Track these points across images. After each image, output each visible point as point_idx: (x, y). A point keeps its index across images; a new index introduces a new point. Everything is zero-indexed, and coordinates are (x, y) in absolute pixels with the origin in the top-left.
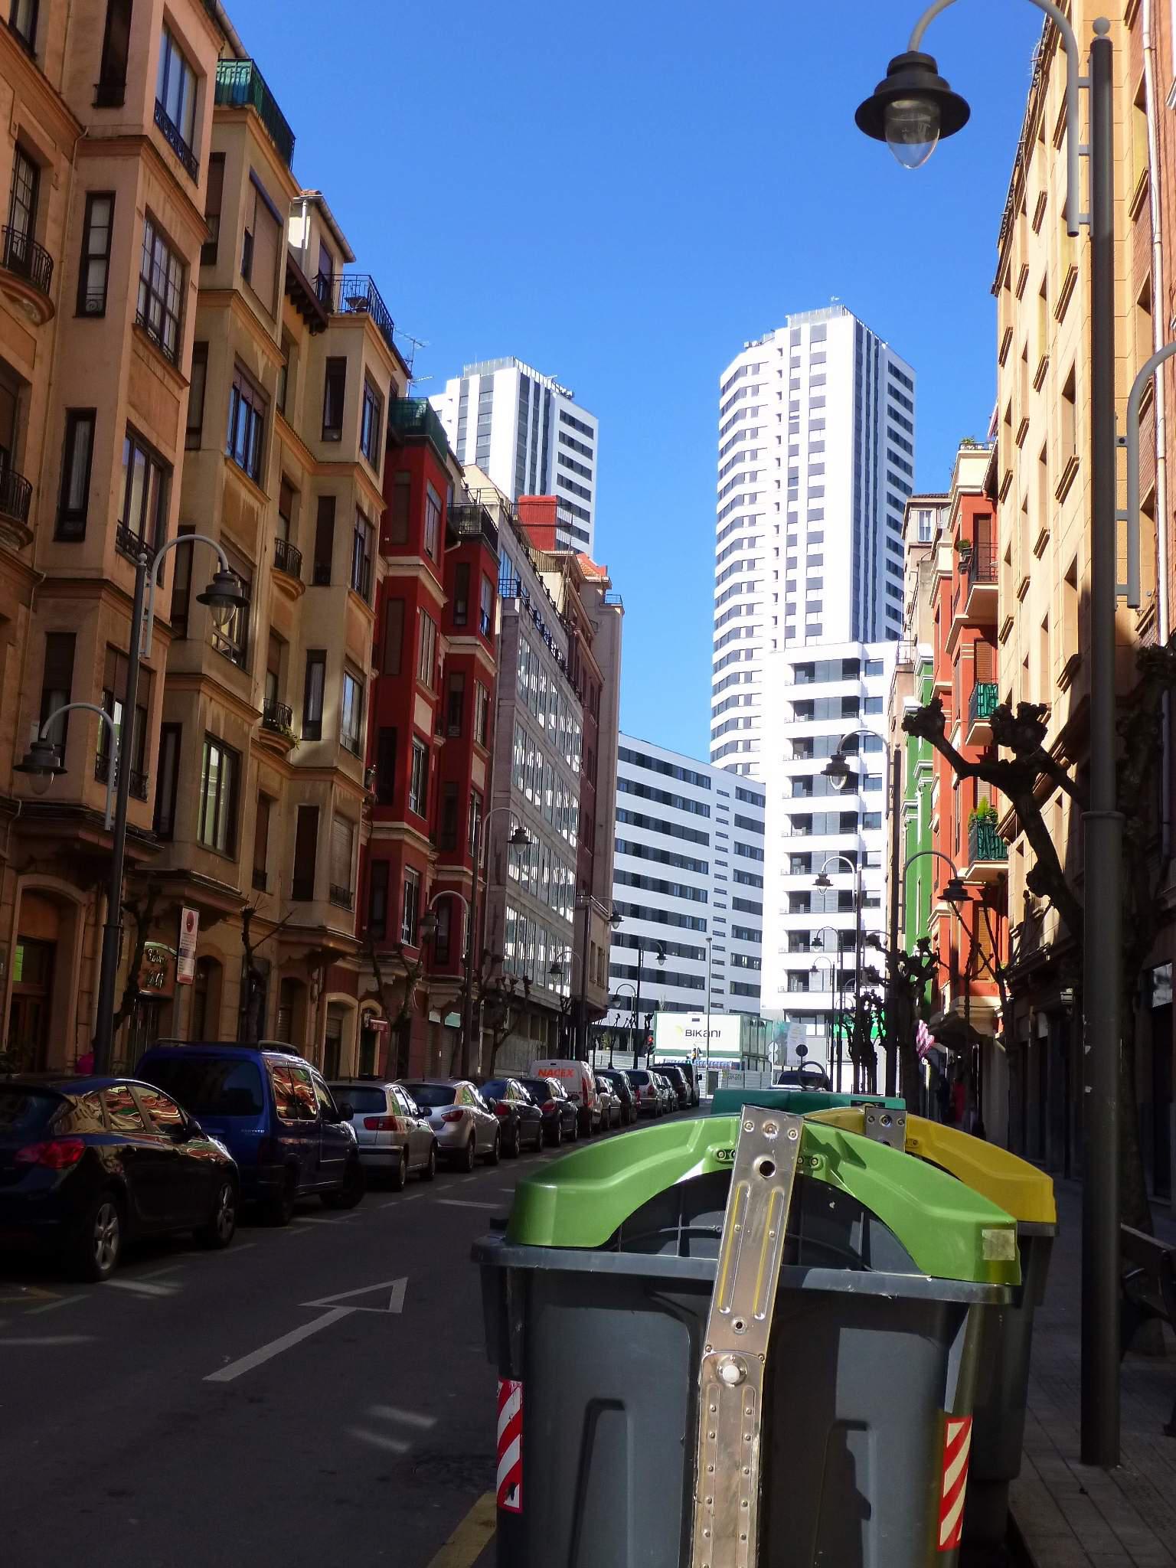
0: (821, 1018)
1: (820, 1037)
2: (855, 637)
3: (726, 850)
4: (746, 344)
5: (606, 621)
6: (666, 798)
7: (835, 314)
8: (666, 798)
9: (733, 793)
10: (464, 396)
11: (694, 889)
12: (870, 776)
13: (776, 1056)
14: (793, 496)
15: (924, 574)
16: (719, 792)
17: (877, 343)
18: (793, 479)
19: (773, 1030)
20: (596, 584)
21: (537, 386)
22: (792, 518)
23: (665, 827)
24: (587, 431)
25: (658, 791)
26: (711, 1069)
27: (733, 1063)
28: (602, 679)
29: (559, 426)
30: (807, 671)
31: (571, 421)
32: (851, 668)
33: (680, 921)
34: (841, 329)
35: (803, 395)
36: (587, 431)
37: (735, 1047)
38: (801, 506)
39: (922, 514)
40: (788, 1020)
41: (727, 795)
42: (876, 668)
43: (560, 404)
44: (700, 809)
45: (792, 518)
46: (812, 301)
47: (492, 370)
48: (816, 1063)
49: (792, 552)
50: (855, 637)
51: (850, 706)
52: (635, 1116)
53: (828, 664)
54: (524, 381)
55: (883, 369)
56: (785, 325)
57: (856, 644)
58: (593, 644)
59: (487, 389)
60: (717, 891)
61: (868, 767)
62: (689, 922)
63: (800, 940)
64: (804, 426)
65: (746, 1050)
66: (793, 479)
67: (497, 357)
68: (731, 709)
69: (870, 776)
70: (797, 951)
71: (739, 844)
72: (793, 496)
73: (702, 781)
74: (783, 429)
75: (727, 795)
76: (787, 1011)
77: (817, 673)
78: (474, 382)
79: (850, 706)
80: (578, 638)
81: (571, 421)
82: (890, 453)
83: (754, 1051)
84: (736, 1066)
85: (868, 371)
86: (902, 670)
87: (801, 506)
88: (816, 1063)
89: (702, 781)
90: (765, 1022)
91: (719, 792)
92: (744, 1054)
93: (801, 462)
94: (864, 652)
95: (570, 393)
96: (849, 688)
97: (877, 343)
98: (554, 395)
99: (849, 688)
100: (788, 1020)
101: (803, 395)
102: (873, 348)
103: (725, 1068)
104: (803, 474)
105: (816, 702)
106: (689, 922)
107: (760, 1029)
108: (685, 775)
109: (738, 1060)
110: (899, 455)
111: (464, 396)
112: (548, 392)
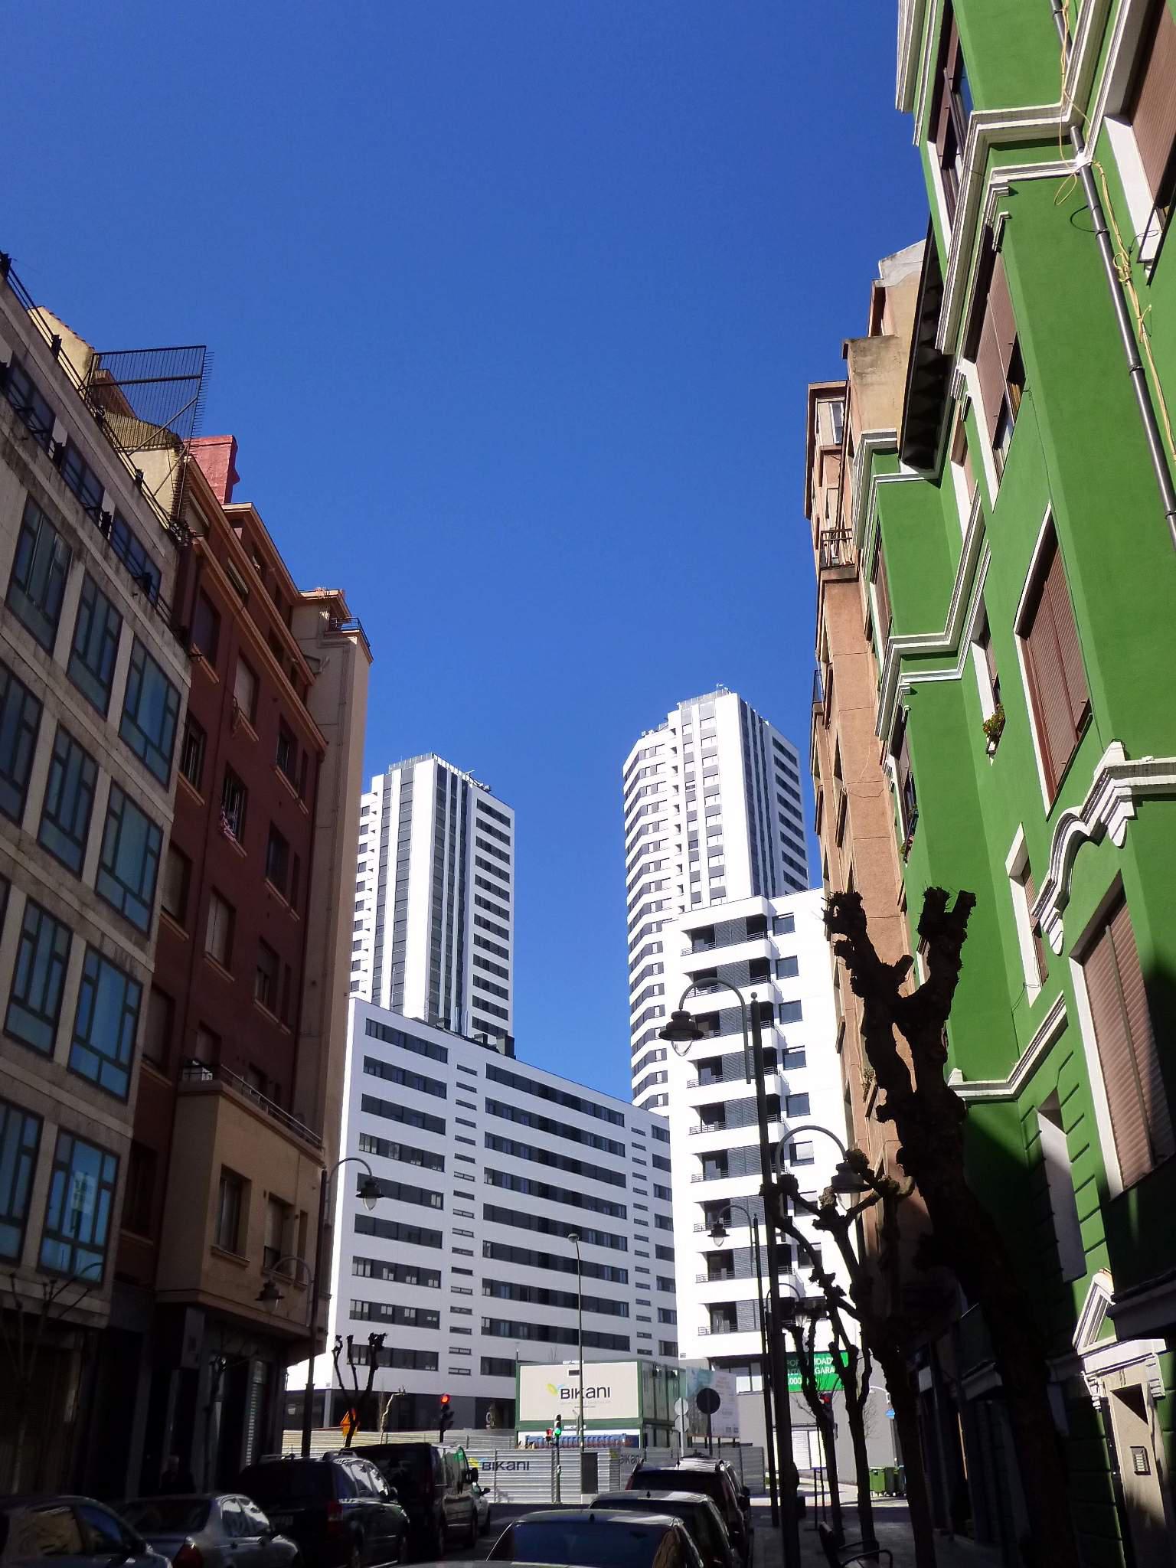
0: (756, 1366)
1: (758, 1393)
2: (756, 892)
3: (645, 1193)
4: (644, 733)
5: (333, 655)
6: (574, 1134)
7: (721, 695)
8: (574, 1134)
9: (649, 1131)
10: (387, 790)
11: (612, 1235)
12: (790, 1051)
13: (687, 1421)
14: (694, 858)
15: (860, 359)
16: (634, 1130)
17: (761, 721)
18: (693, 843)
19: (689, 1385)
20: (320, 603)
21: (454, 777)
22: (695, 877)
23: (575, 1166)
24: (505, 821)
25: (565, 1126)
26: (588, 1450)
27: (628, 1437)
28: (323, 744)
29: (475, 813)
30: (705, 937)
31: (489, 810)
32: (756, 926)
33: (596, 1271)
34: (725, 708)
35: (697, 768)
36: (505, 821)
37: (634, 1412)
38: (702, 866)
39: (836, 408)
40: (713, 1369)
41: (643, 1134)
42: (785, 924)
43: (477, 794)
44: (615, 1148)
45: (695, 877)
46: (699, 686)
47: (413, 764)
48: (362, 1162)
49: (696, 887)
50: (756, 892)
51: (759, 970)
52: (478, 1533)
53: (726, 925)
54: (441, 773)
55: (770, 763)
56: (677, 708)
57: (760, 899)
58: (313, 693)
59: (407, 784)
60: (638, 1237)
61: (783, 995)
62: (608, 1273)
63: (721, 1264)
64: (700, 793)
65: (650, 1415)
66: (693, 843)
67: (418, 755)
68: (650, 1064)
69: (790, 1051)
70: (719, 1278)
71: (660, 1187)
72: (694, 858)
73: (615, 1118)
74: (681, 799)
75: (643, 1134)
76: (712, 1360)
77: (717, 936)
78: (396, 776)
79: (759, 970)
80: (202, 558)
81: (489, 810)
82: (779, 797)
83: (662, 1416)
84: (632, 1441)
85: (763, 841)
86: (834, 577)
87: (702, 866)
88: (362, 1162)
89: (615, 1118)
90: (676, 1372)
91: (634, 1130)
92: (646, 1422)
93: (700, 826)
94: (770, 907)
95: (487, 787)
96: (754, 949)
97: (761, 721)
98: (471, 786)
99: (754, 949)
100: (713, 1369)
101: (697, 768)
102: (758, 725)
103: (612, 1444)
104: (702, 837)
105: (719, 971)
106: (608, 1273)
107: (671, 1383)
108: (596, 1111)
109: (636, 1432)
110: (795, 878)
111: (387, 790)
112: (465, 783)
